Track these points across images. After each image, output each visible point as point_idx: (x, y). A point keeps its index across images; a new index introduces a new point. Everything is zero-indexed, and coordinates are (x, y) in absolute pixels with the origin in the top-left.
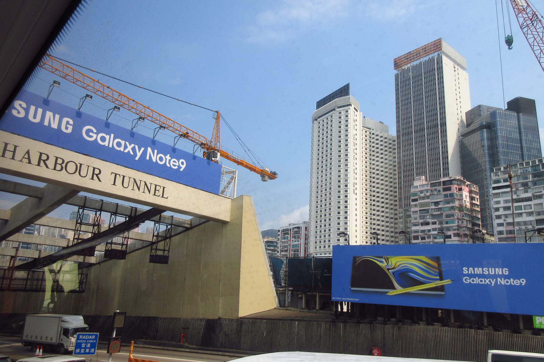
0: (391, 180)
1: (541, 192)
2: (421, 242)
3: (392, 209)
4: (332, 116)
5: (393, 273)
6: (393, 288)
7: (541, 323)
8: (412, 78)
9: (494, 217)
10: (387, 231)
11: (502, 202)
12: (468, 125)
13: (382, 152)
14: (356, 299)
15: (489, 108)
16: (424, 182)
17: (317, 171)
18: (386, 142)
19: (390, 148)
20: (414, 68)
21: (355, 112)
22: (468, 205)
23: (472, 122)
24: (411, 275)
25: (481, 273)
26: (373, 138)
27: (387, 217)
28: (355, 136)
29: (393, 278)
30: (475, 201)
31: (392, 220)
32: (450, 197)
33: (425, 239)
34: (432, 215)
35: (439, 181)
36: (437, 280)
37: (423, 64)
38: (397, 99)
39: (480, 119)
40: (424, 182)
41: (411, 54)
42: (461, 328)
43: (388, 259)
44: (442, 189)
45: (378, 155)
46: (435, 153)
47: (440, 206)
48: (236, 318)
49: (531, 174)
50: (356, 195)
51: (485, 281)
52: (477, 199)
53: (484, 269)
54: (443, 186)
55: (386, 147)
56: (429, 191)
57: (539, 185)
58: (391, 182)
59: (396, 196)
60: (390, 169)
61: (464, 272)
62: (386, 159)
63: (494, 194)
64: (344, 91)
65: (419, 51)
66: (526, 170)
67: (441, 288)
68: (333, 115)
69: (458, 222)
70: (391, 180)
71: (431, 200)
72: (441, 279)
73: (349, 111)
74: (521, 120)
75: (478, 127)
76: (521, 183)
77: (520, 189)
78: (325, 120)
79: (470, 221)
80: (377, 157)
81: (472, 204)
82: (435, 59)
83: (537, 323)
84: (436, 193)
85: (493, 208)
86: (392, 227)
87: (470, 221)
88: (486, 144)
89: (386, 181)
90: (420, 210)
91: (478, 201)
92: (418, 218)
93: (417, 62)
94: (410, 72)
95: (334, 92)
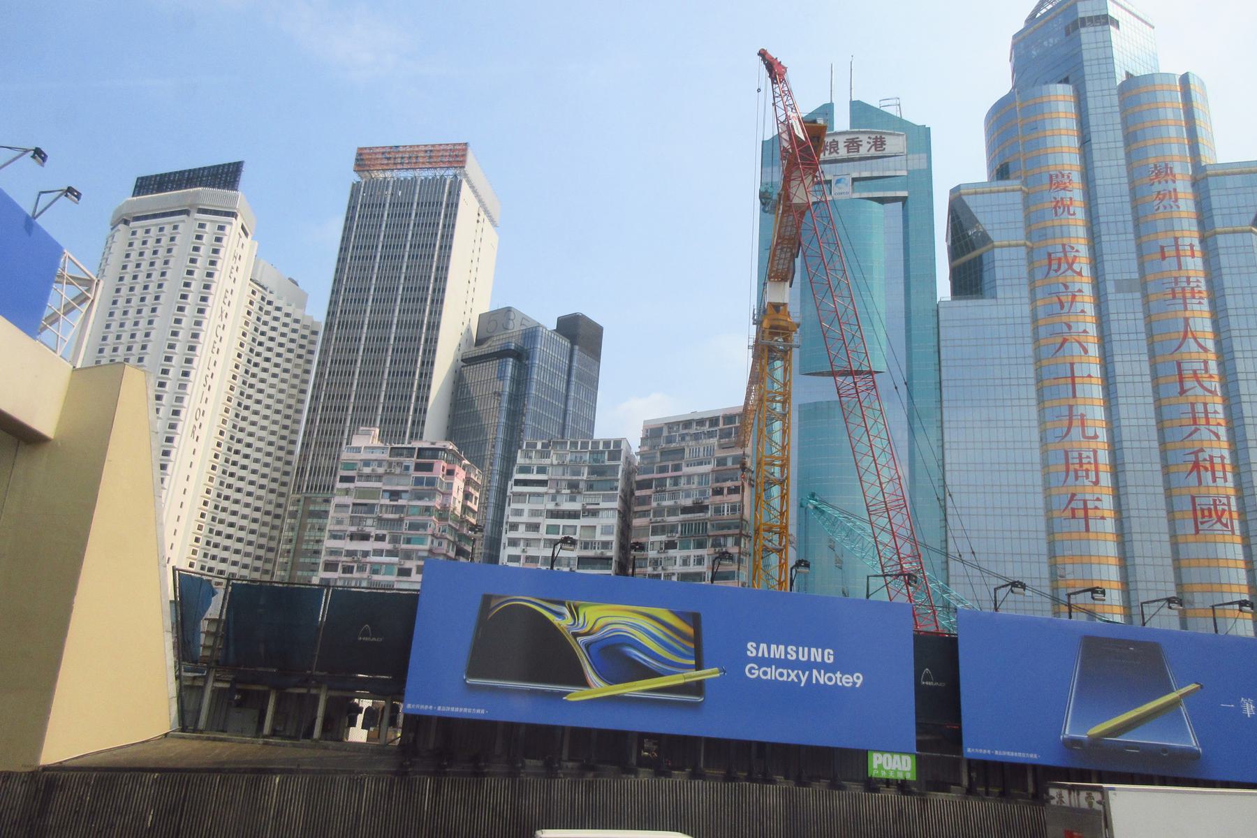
0: (288, 422)
1: (598, 504)
2: (340, 578)
3: (272, 491)
4: (175, 227)
5: (588, 646)
6: (583, 682)
7: (880, 767)
8: (390, 205)
9: (504, 539)
10: (250, 543)
11: (526, 513)
12: (479, 342)
13: (281, 350)
14: (478, 711)
15: (524, 318)
16: (376, 443)
17: (97, 357)
18: (294, 331)
19: (302, 347)
20: (399, 184)
21: (241, 237)
22: (459, 507)
23: (488, 338)
24: (630, 652)
25: (783, 657)
26: (268, 313)
27: (257, 509)
28: (229, 295)
29: (584, 658)
30: (471, 501)
31: (268, 519)
32: (427, 485)
33: (352, 572)
34: (380, 519)
35: (410, 446)
36: (688, 667)
37: (419, 182)
38: (345, 239)
39: (505, 336)
40: (376, 443)
41: (399, 152)
42: (732, 781)
43: (577, 609)
44: (414, 464)
45: (269, 355)
46: (404, 384)
47: (401, 502)
48: (29, 769)
49: (589, 466)
50: (197, 440)
51: (789, 675)
52: (476, 498)
53: (789, 649)
54: (417, 458)
55: (292, 341)
56: (384, 463)
57: (597, 490)
58: (285, 427)
59: (288, 463)
60: (291, 396)
61: (749, 653)
62: (286, 371)
63: (515, 494)
64: (226, 176)
65: (417, 152)
66: (581, 458)
67: (696, 688)
68: (181, 226)
69: (432, 542)
70: (288, 422)
71: (384, 484)
72: (698, 666)
73: (228, 228)
74: (576, 358)
75: (496, 350)
76: (569, 480)
77: (563, 491)
78: (154, 231)
79: (454, 543)
80: (267, 360)
81: (466, 509)
82: (448, 182)
83: (875, 766)
84: (398, 471)
85: (507, 523)
86: (263, 535)
87: (454, 543)
88: (507, 390)
89: (275, 422)
90: (354, 504)
91: (475, 504)
92: (347, 521)
93: (409, 175)
94: (387, 190)
95: (195, 170)
